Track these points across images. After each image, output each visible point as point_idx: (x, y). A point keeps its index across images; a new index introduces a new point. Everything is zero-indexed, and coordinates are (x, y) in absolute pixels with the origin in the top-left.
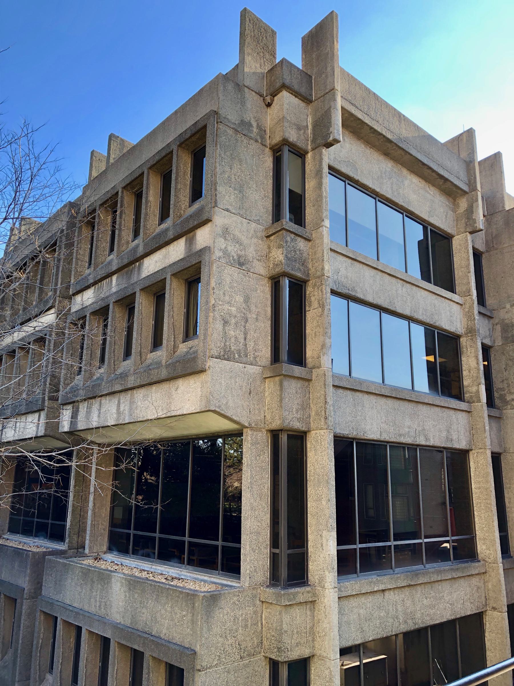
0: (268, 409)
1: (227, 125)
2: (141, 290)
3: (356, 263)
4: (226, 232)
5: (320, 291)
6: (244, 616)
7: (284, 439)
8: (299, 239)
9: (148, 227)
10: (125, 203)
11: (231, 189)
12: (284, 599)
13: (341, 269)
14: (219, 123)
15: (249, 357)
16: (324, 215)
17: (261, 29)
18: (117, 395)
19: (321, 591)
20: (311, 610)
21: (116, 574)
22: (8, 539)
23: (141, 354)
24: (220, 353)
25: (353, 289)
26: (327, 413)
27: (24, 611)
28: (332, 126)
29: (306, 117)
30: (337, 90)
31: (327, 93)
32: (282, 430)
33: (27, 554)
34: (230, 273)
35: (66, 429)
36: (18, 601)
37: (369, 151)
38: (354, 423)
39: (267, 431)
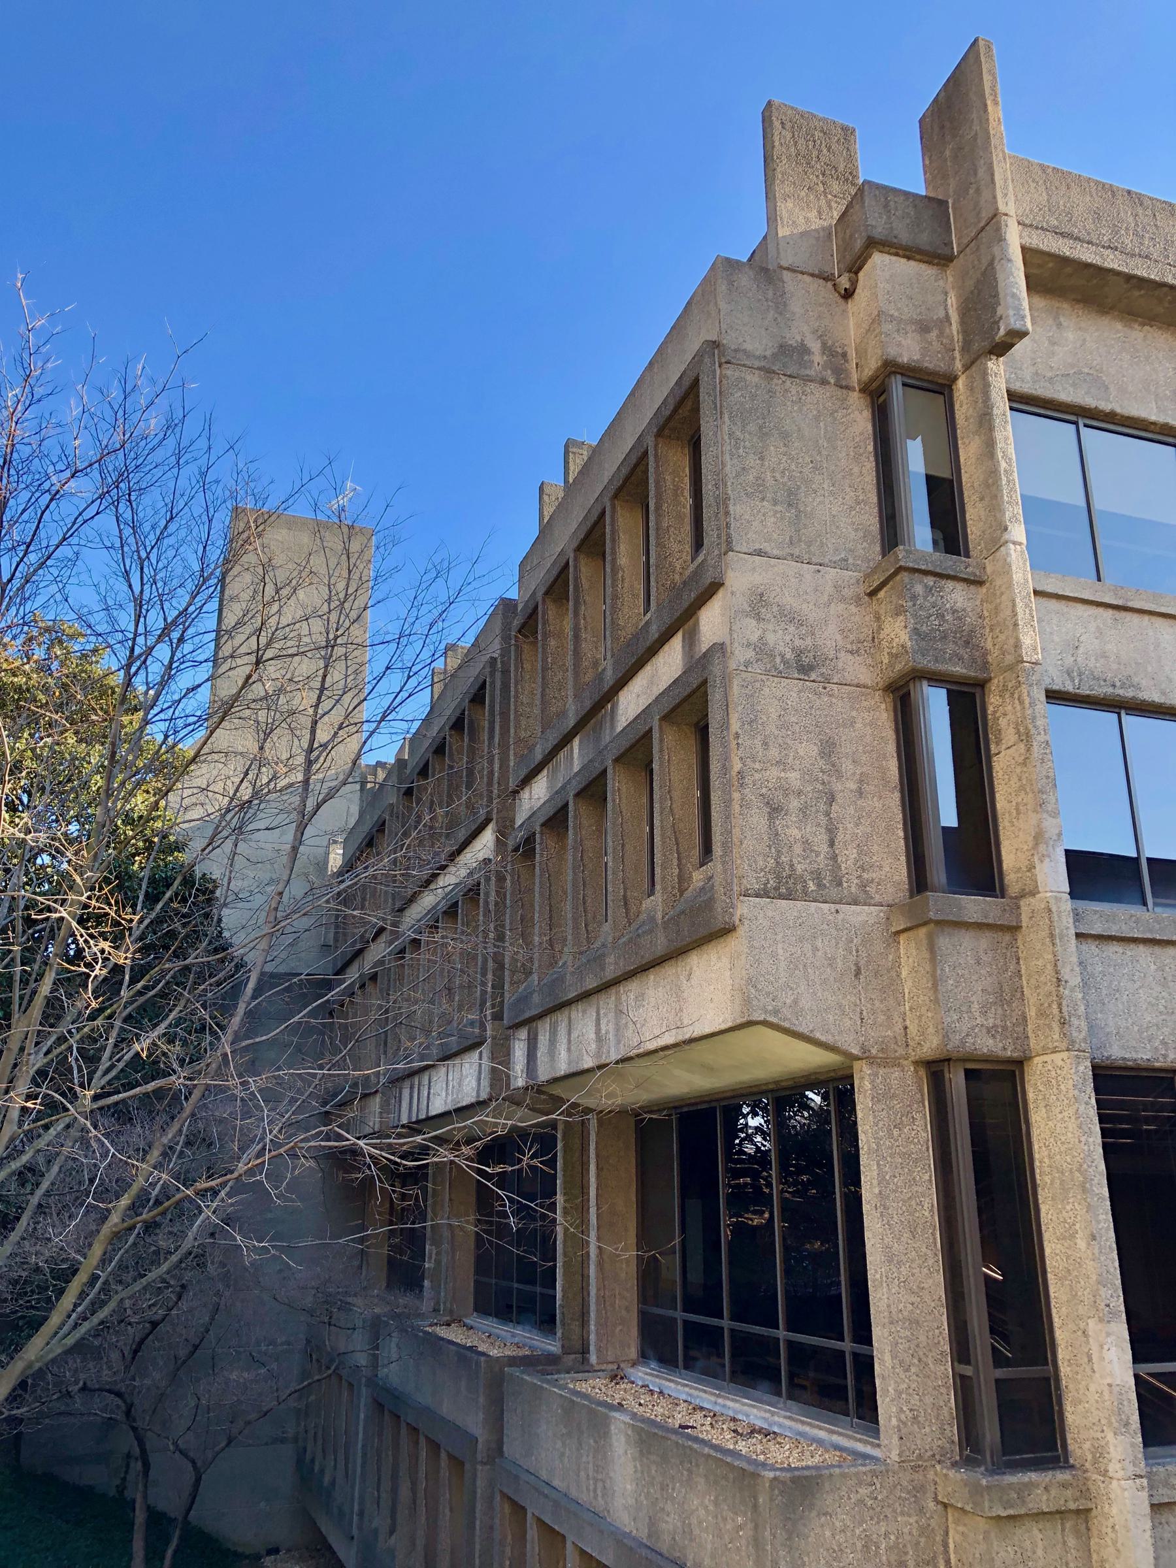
0: (911, 1010)
1: (744, 365)
2: (617, 760)
3: (1128, 616)
4: (758, 603)
5: (1017, 701)
6: (892, 1537)
7: (957, 1081)
8: (950, 584)
9: (621, 622)
10: (584, 581)
11: (765, 503)
12: (991, 1501)
13: (1082, 639)
14: (725, 366)
15: (845, 885)
16: (1008, 515)
17: (813, 135)
18: (594, 998)
19: (1102, 1485)
20: (1077, 1534)
21: (616, 1415)
22: (472, 1328)
23: (626, 904)
24: (765, 884)
25: (1127, 683)
26: (1065, 1009)
27: (479, 1491)
28: (1002, 302)
29: (941, 297)
30: (1006, 215)
31: (983, 228)
32: (949, 1060)
33: (477, 1363)
34: (779, 694)
35: (520, 1083)
36: (467, 1466)
37: (1138, 335)
38: (1166, 1030)
39: (916, 1063)
